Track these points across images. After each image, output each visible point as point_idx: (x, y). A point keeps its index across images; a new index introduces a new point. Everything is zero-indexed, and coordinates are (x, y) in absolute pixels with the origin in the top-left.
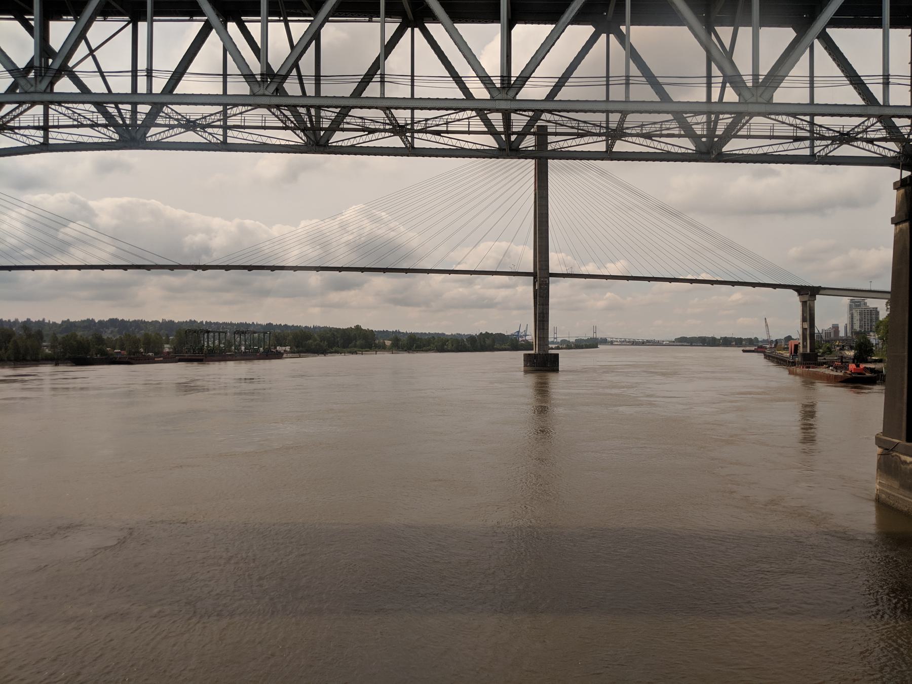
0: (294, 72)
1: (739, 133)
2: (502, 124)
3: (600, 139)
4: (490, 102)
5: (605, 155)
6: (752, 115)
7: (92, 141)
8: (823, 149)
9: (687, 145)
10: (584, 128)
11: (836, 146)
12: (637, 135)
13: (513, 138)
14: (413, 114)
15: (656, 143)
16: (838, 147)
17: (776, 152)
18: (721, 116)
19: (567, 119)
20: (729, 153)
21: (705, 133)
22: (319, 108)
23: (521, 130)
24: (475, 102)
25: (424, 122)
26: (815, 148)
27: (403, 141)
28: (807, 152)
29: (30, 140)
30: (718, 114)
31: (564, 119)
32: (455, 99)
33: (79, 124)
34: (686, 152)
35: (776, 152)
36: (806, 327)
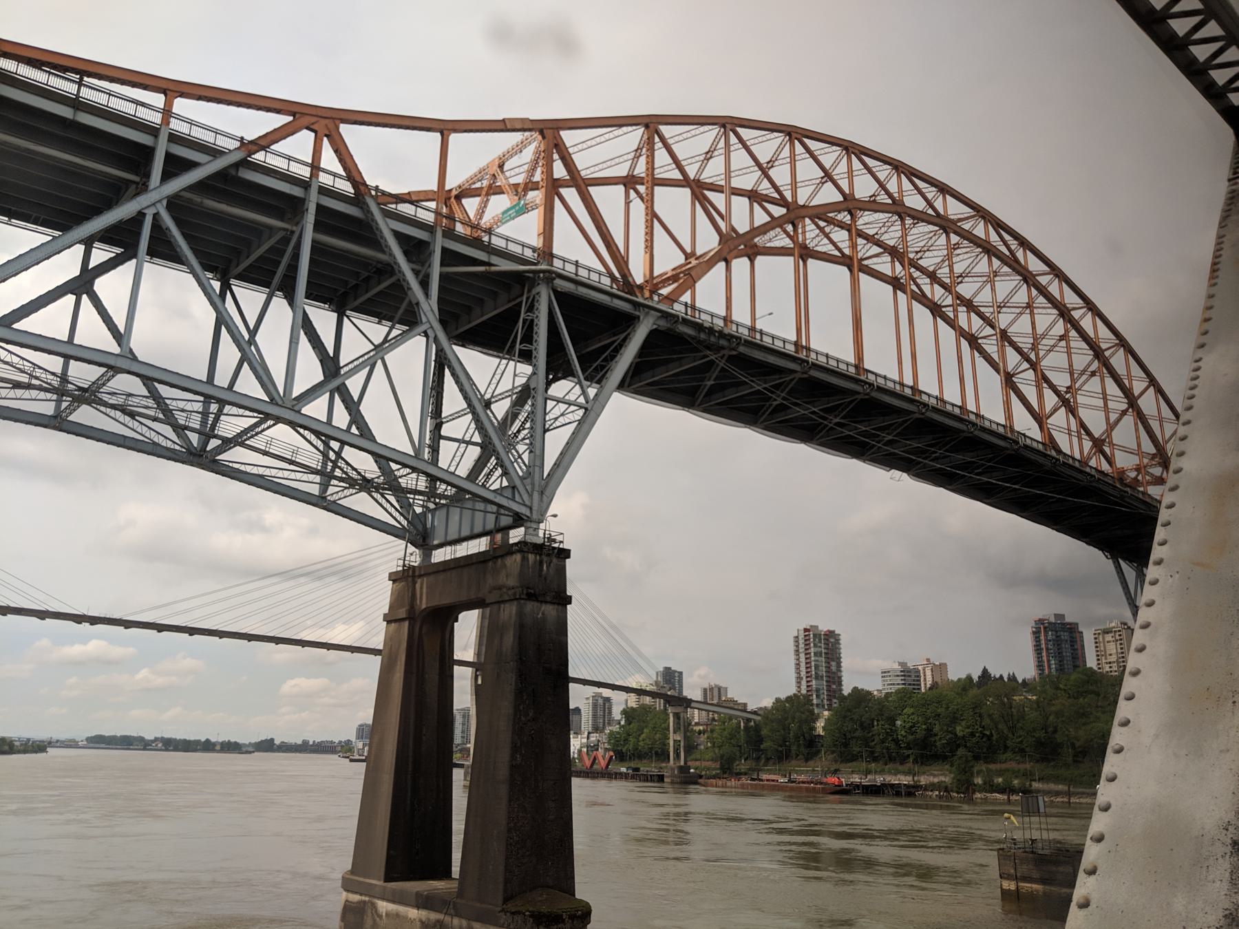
0: (1113, 417)
1: (247, 442)
2: (200, 419)
3: (49, 396)
4: (66, 345)
5: (314, 500)
6: (278, 420)
7: (257, 472)
8: (343, 490)
9: (165, 434)
10: (53, 382)
11: (354, 491)
12: (113, 407)
13: (214, 443)
14: (66, 367)
15: (136, 424)
16: (356, 493)
17: (274, 477)
18: (227, 409)
19: (31, 365)
20: (227, 463)
21: (319, 468)
22: (222, 403)
23: (230, 436)
24: (11, 331)
25: (124, 397)
26: (330, 487)
27: (75, 410)
28: (315, 490)
29: (149, 436)
30: (222, 403)
31: (25, 363)
32: (40, 335)
33: (344, 476)
34: (172, 447)
35: (274, 477)
36: (679, 739)
